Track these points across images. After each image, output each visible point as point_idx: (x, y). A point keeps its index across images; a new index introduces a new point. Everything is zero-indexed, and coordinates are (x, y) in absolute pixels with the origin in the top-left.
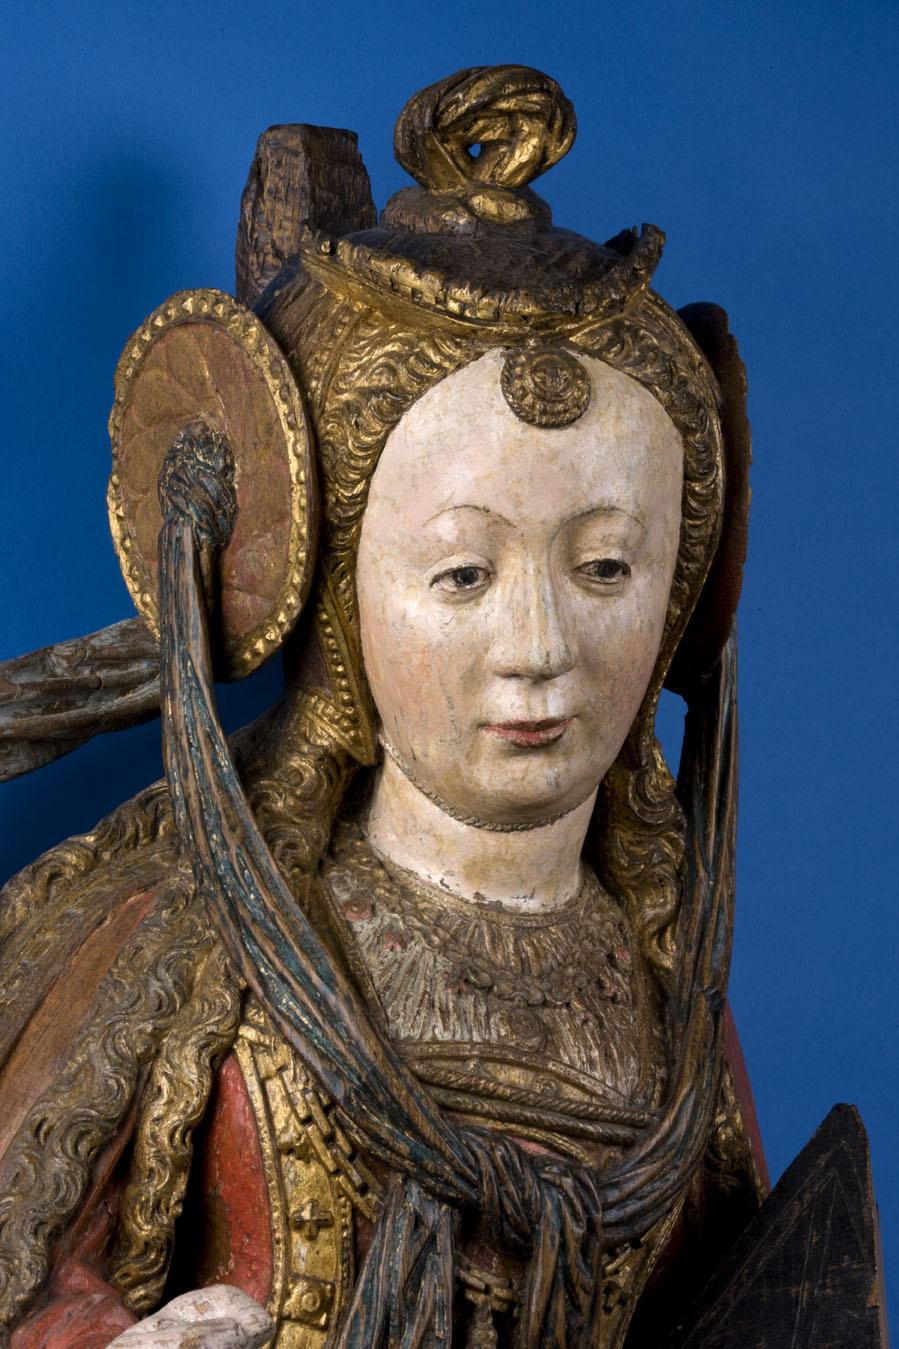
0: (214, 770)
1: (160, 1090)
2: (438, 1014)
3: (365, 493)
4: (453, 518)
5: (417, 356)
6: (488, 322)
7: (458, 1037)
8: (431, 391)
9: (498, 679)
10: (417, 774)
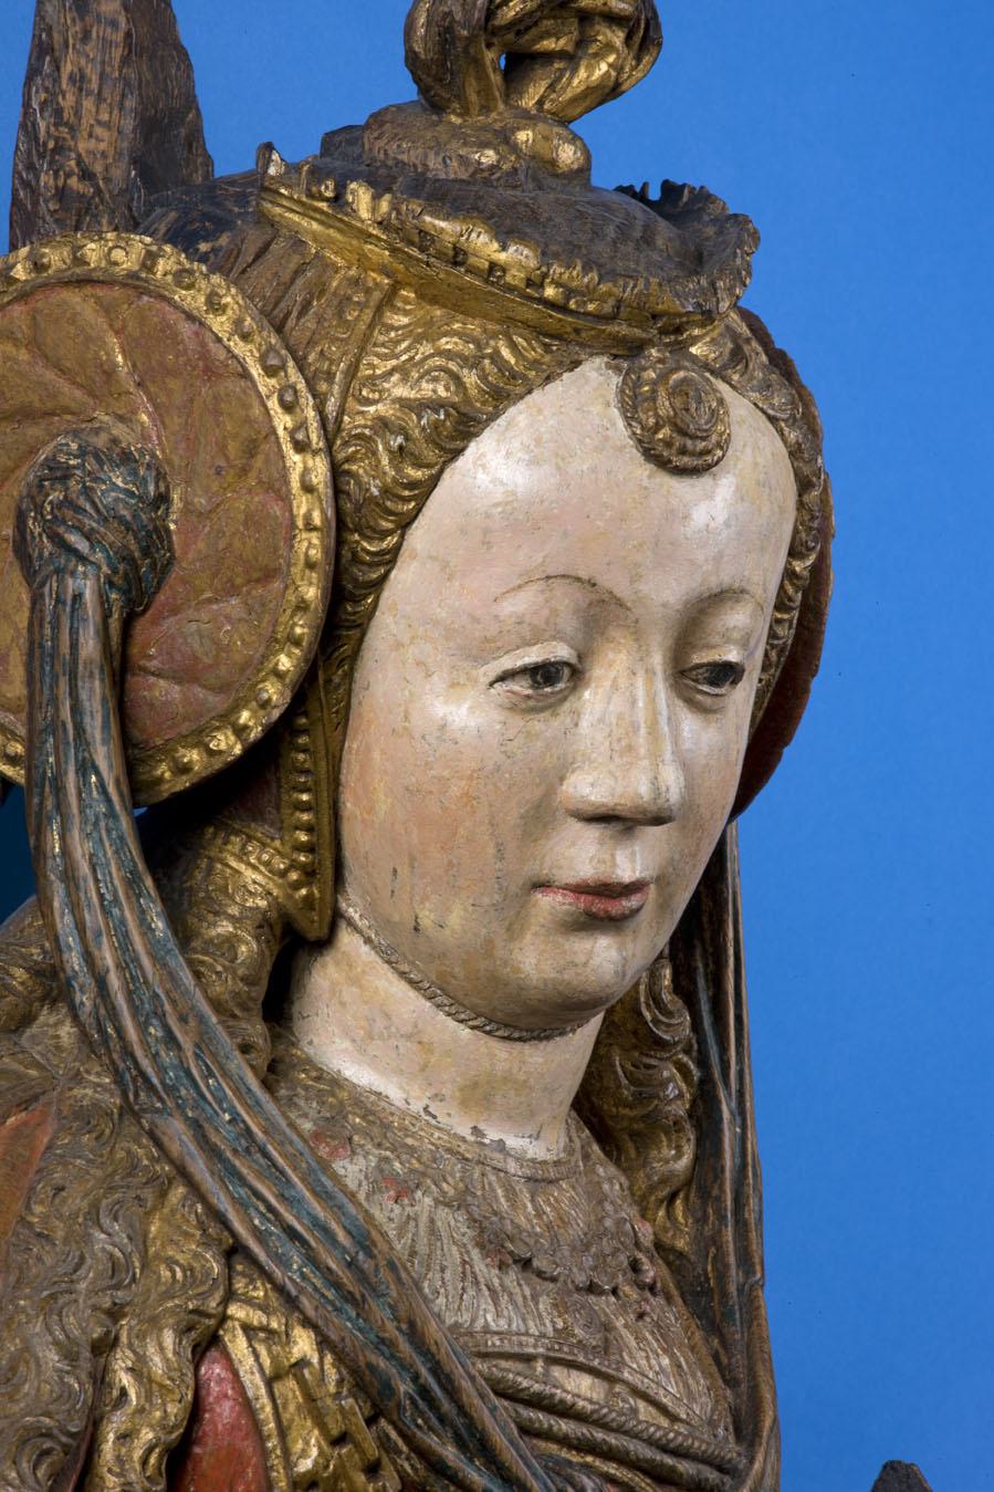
0: (143, 934)
1: (124, 1392)
2: (487, 1293)
3: (397, 548)
4: (542, 592)
5: (491, 357)
6: (598, 317)
7: (514, 1326)
8: (512, 411)
10: (408, 954)
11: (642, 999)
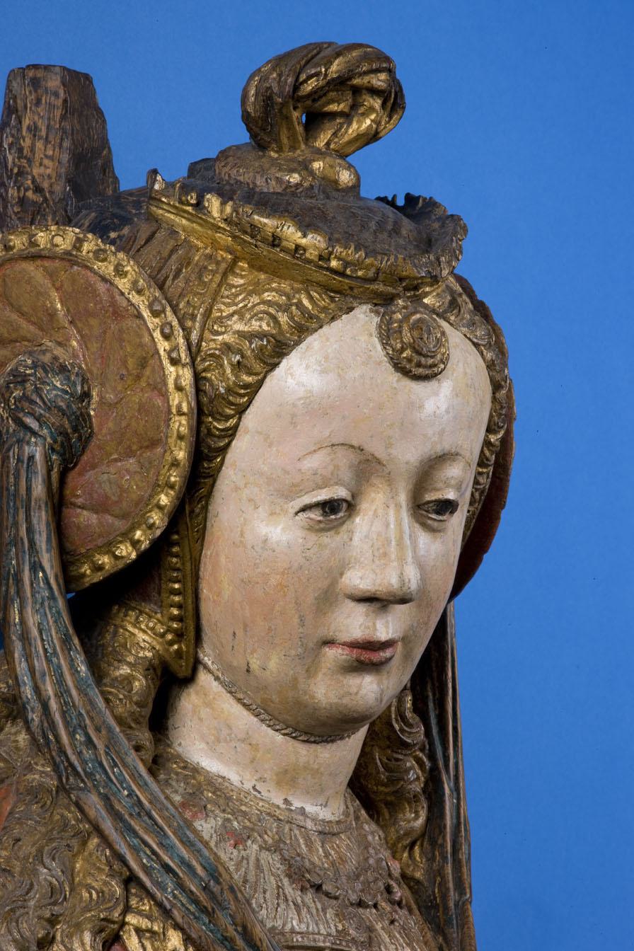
0: (72, 675)
2: (293, 907)
4: (329, 454)
5: (296, 305)
8: (310, 339)
9: (351, 605)
11: (393, 716)
